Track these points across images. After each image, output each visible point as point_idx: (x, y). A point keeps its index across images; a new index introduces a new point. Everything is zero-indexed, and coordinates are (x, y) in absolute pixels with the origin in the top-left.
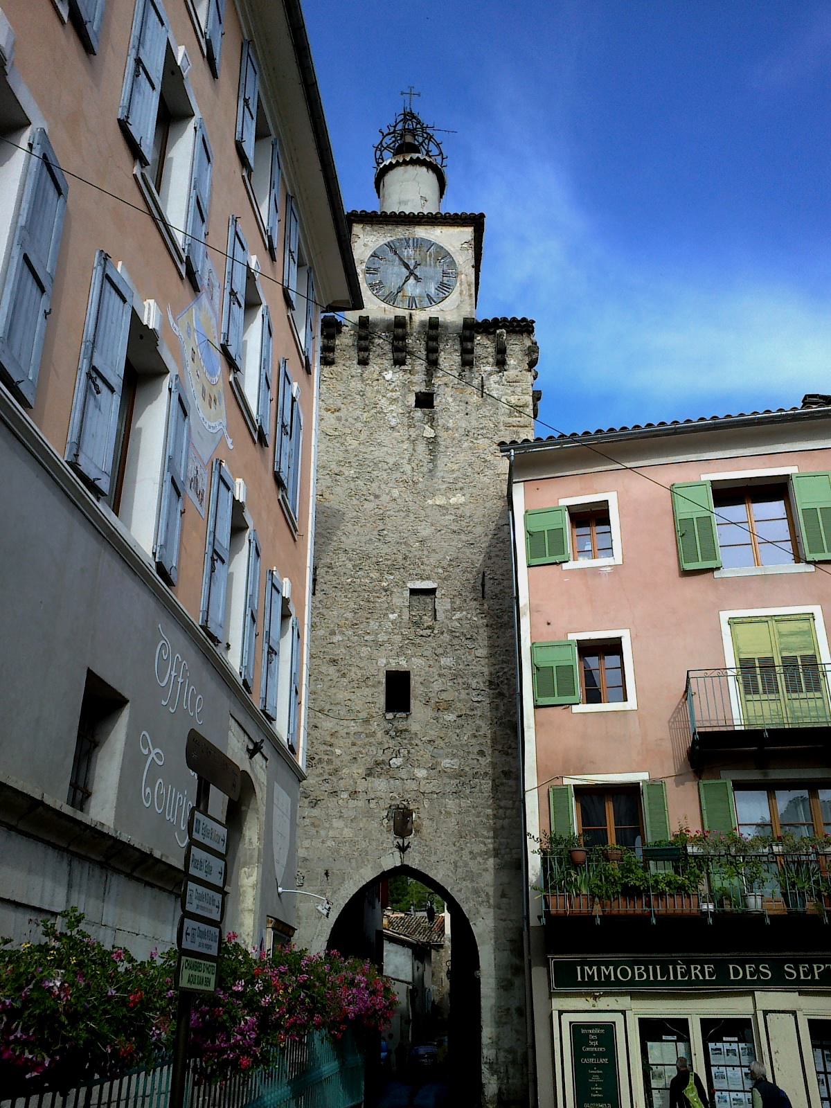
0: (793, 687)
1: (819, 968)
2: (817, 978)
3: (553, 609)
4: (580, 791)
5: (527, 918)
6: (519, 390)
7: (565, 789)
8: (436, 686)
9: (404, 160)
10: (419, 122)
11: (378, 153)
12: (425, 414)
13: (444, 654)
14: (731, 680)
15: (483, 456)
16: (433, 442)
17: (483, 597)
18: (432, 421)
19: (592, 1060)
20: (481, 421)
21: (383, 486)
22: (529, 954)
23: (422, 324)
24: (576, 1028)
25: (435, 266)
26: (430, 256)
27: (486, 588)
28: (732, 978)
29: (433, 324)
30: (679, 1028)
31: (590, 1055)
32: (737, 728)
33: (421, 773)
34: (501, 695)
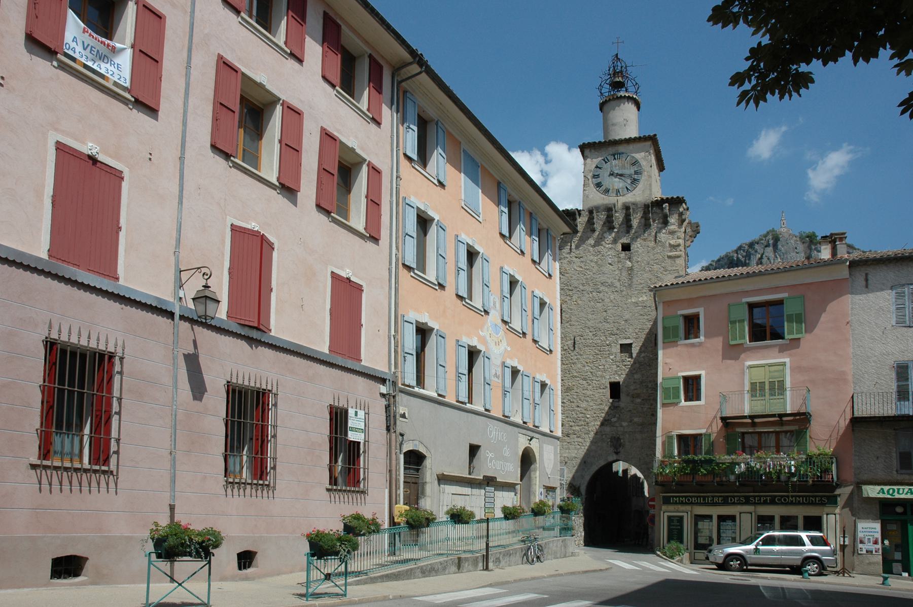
3: (672, 364)
4: (681, 438)
8: (632, 388)
13: (636, 373)
16: (631, 269)
18: (630, 259)
30: (709, 517)
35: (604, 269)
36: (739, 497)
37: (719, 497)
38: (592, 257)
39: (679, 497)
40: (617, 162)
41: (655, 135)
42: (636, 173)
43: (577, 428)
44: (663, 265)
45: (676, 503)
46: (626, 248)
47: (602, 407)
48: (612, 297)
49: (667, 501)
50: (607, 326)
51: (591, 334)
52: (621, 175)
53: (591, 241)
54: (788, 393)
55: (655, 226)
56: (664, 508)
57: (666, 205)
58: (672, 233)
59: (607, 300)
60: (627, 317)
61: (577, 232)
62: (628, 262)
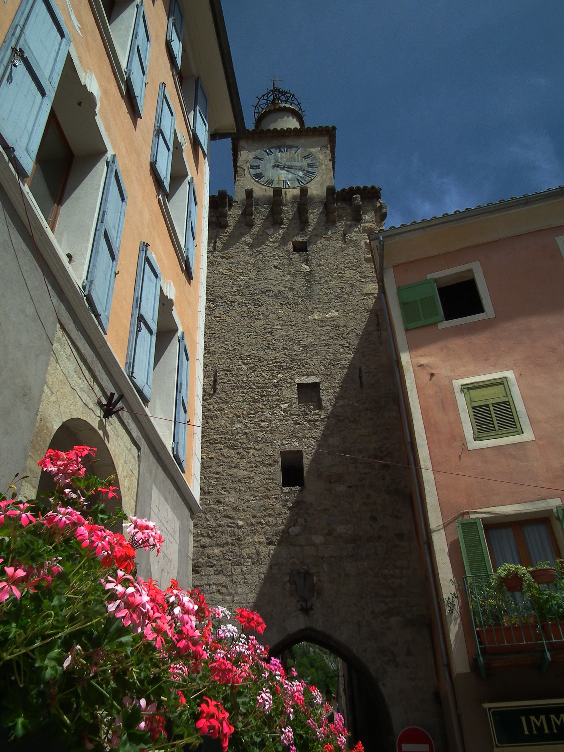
4: (493, 526)
5: (449, 666)
12: (301, 256)
15: (350, 282)
16: (310, 274)
18: (307, 262)
20: (346, 258)
21: (270, 308)
25: (302, 161)
26: (298, 156)
27: (364, 379)
38: (247, 258)
41: (334, 128)
43: (216, 551)
44: (359, 269)
47: (267, 502)
50: (274, 354)
51: (245, 367)
53: (247, 239)
55: (341, 225)
57: (358, 197)
59: (272, 316)
60: (308, 341)
61: (225, 226)
62: (304, 265)
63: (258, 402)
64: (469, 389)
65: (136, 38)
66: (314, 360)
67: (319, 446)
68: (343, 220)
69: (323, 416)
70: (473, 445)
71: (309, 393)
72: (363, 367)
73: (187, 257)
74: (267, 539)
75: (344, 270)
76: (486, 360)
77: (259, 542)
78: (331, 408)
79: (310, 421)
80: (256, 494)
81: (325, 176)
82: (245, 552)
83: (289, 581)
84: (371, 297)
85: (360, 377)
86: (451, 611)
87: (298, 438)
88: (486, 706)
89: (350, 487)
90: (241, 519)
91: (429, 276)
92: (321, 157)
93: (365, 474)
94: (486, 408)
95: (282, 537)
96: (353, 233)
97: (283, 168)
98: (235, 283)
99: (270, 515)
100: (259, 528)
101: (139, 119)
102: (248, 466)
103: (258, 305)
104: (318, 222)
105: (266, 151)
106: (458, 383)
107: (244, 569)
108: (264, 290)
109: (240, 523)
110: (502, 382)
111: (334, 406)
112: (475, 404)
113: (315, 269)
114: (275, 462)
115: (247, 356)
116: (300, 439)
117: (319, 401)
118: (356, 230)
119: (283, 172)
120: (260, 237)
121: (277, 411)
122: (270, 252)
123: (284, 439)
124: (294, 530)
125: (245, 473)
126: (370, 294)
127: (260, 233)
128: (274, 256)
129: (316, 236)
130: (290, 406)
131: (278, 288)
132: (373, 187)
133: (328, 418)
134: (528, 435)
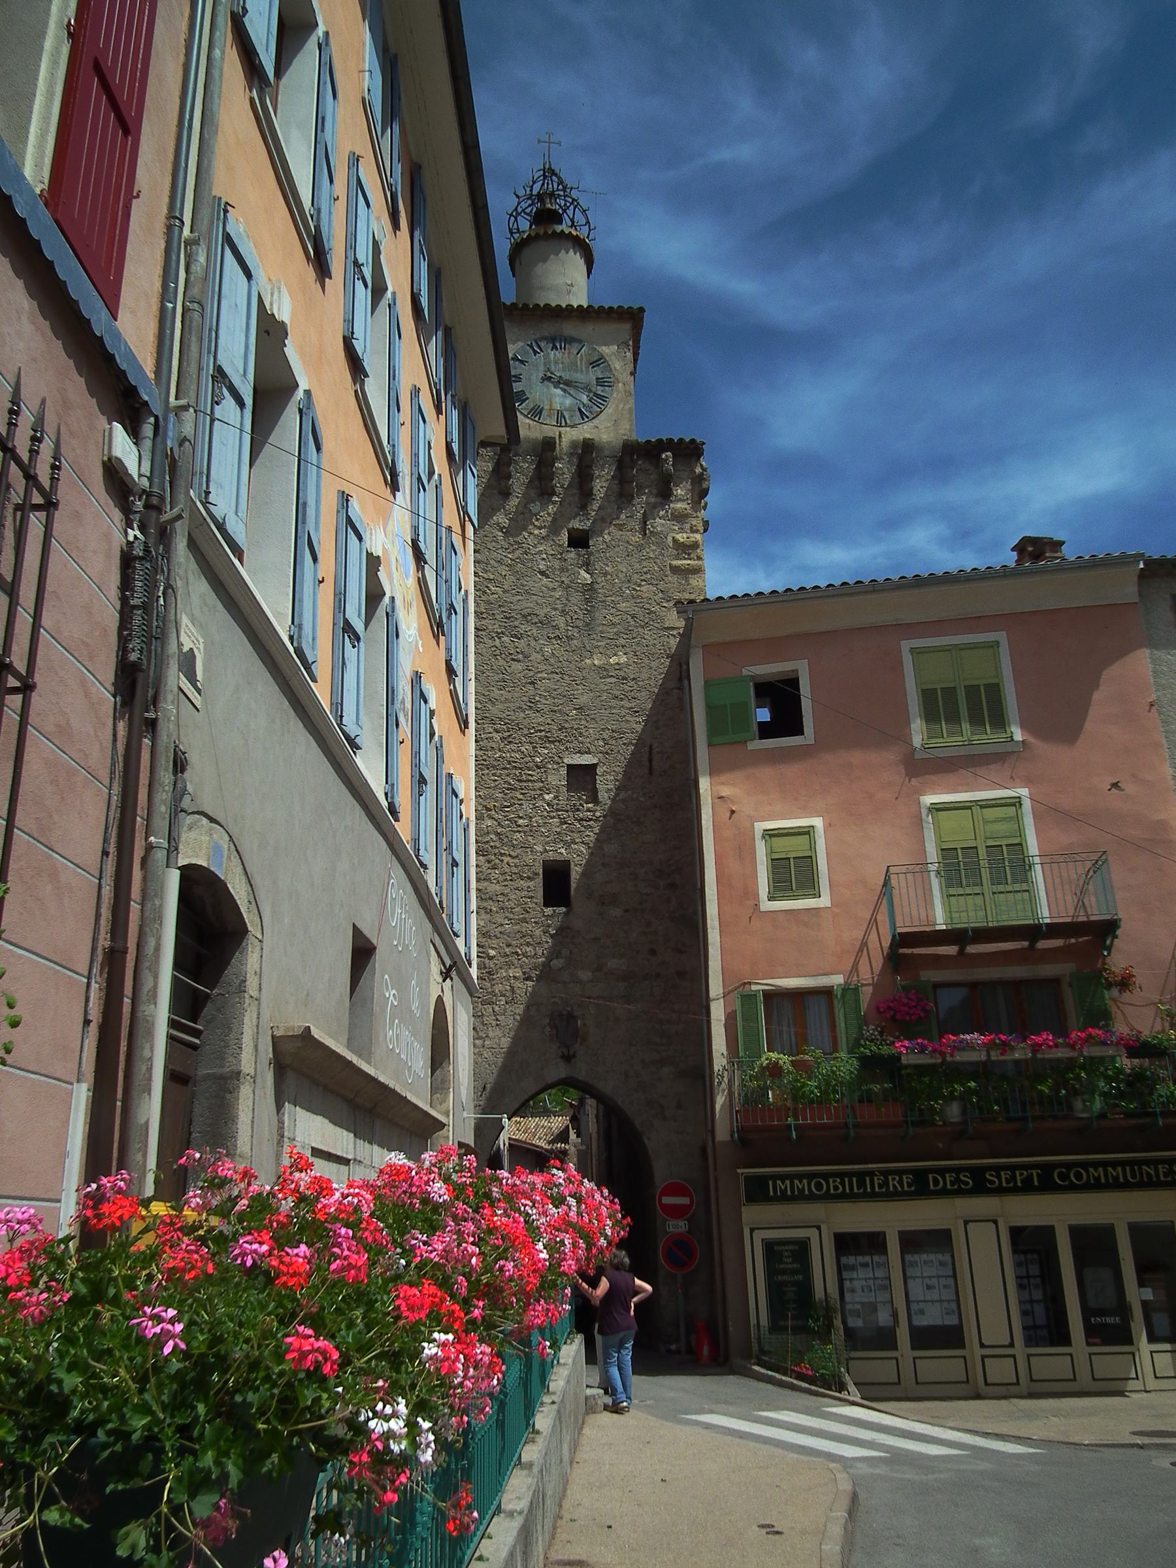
0: (998, 878)
1: (1021, 1174)
2: (1019, 1184)
4: (772, 997)
5: (713, 1131)
6: (688, 526)
7: (753, 996)
9: (546, 232)
10: (560, 182)
11: (513, 219)
12: (579, 555)
14: (933, 874)
15: (647, 606)
16: (591, 588)
17: (651, 773)
18: (587, 566)
19: (786, 1278)
20: (645, 564)
21: (533, 643)
22: (715, 1169)
23: (574, 444)
24: (770, 1247)
25: (587, 371)
26: (581, 360)
27: (654, 763)
28: (932, 1187)
29: (587, 451)
30: (873, 1243)
31: (783, 1272)
32: (938, 928)
33: (585, 975)
34: (672, 886)
35: (529, 583)
36: (958, 1170)
37: (900, 1172)
39: (1104, 1164)
40: (559, 354)
42: (600, 382)
44: (662, 585)
45: (784, 1198)
46: (579, 541)
48: (548, 650)
49: (758, 1192)
51: (497, 736)
52: (568, 383)
53: (501, 518)
54: (1038, 874)
55: (641, 502)
56: (751, 1214)
57: (667, 455)
58: (680, 518)
59: (536, 657)
60: (584, 699)
63: (515, 789)
64: (771, 836)
65: (323, 131)
66: (591, 731)
67: (591, 854)
68: (644, 494)
69: (598, 814)
70: (767, 905)
71: (582, 778)
72: (656, 745)
73: (318, 228)
74: (524, 973)
75: (640, 586)
76: (796, 799)
77: (515, 977)
78: (609, 802)
79: (582, 820)
80: (511, 916)
81: (621, 406)
82: (498, 988)
83: (549, 1024)
84: (675, 632)
85: (650, 761)
86: (720, 1083)
87: (565, 842)
88: (739, 1171)
89: (626, 911)
90: (493, 948)
91: (745, 672)
92: (618, 366)
93: (646, 894)
94: (785, 862)
95: (541, 971)
96: (658, 520)
97: (557, 385)
98: (484, 598)
99: (528, 944)
100: (514, 959)
101: (327, 280)
102: (501, 878)
103: (516, 636)
104: (606, 494)
105: (531, 346)
106: (761, 826)
107: (497, 1008)
108: (525, 612)
109: (492, 953)
110: (808, 832)
111: (613, 800)
112: (775, 856)
113: (599, 580)
114: (536, 874)
115: (501, 719)
116: (568, 845)
117: (595, 791)
118: (662, 513)
119: (558, 391)
120: (521, 517)
121: (540, 803)
122: (535, 546)
123: (547, 843)
124: (557, 963)
125: (498, 887)
126: (673, 628)
127: (521, 509)
128: (540, 552)
129: (603, 520)
130: (556, 797)
131: (545, 611)
132: (693, 441)
133: (604, 816)
134: (824, 901)
